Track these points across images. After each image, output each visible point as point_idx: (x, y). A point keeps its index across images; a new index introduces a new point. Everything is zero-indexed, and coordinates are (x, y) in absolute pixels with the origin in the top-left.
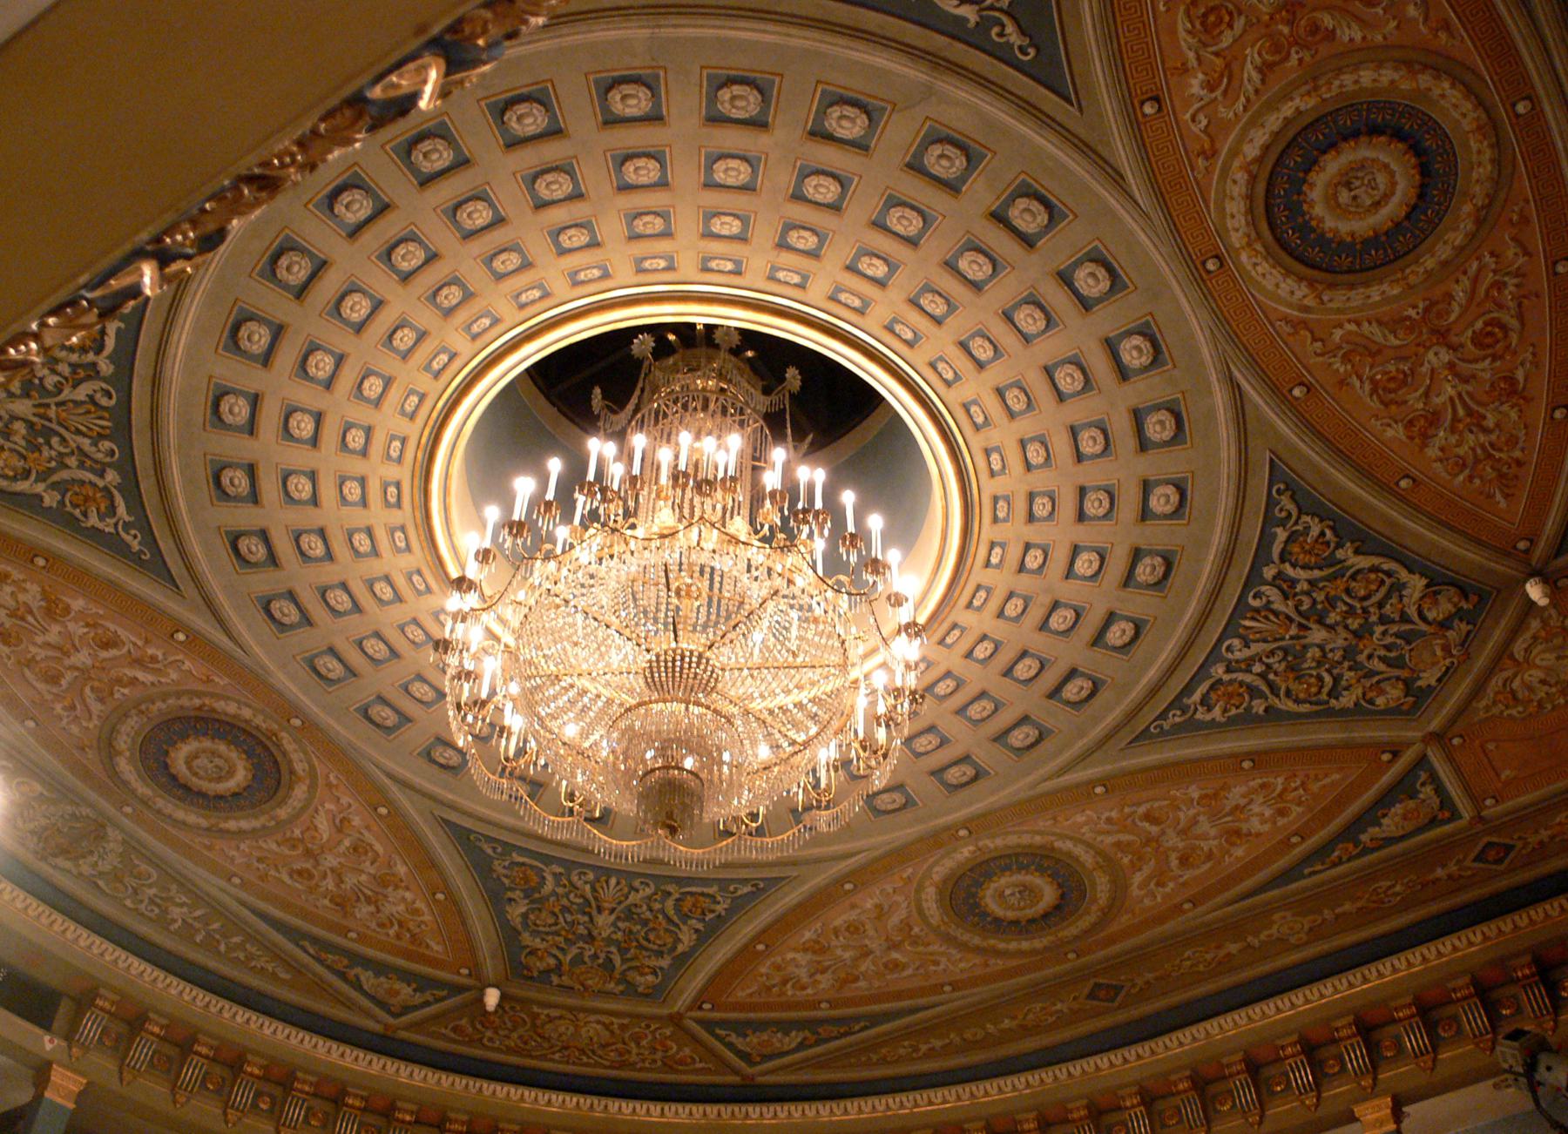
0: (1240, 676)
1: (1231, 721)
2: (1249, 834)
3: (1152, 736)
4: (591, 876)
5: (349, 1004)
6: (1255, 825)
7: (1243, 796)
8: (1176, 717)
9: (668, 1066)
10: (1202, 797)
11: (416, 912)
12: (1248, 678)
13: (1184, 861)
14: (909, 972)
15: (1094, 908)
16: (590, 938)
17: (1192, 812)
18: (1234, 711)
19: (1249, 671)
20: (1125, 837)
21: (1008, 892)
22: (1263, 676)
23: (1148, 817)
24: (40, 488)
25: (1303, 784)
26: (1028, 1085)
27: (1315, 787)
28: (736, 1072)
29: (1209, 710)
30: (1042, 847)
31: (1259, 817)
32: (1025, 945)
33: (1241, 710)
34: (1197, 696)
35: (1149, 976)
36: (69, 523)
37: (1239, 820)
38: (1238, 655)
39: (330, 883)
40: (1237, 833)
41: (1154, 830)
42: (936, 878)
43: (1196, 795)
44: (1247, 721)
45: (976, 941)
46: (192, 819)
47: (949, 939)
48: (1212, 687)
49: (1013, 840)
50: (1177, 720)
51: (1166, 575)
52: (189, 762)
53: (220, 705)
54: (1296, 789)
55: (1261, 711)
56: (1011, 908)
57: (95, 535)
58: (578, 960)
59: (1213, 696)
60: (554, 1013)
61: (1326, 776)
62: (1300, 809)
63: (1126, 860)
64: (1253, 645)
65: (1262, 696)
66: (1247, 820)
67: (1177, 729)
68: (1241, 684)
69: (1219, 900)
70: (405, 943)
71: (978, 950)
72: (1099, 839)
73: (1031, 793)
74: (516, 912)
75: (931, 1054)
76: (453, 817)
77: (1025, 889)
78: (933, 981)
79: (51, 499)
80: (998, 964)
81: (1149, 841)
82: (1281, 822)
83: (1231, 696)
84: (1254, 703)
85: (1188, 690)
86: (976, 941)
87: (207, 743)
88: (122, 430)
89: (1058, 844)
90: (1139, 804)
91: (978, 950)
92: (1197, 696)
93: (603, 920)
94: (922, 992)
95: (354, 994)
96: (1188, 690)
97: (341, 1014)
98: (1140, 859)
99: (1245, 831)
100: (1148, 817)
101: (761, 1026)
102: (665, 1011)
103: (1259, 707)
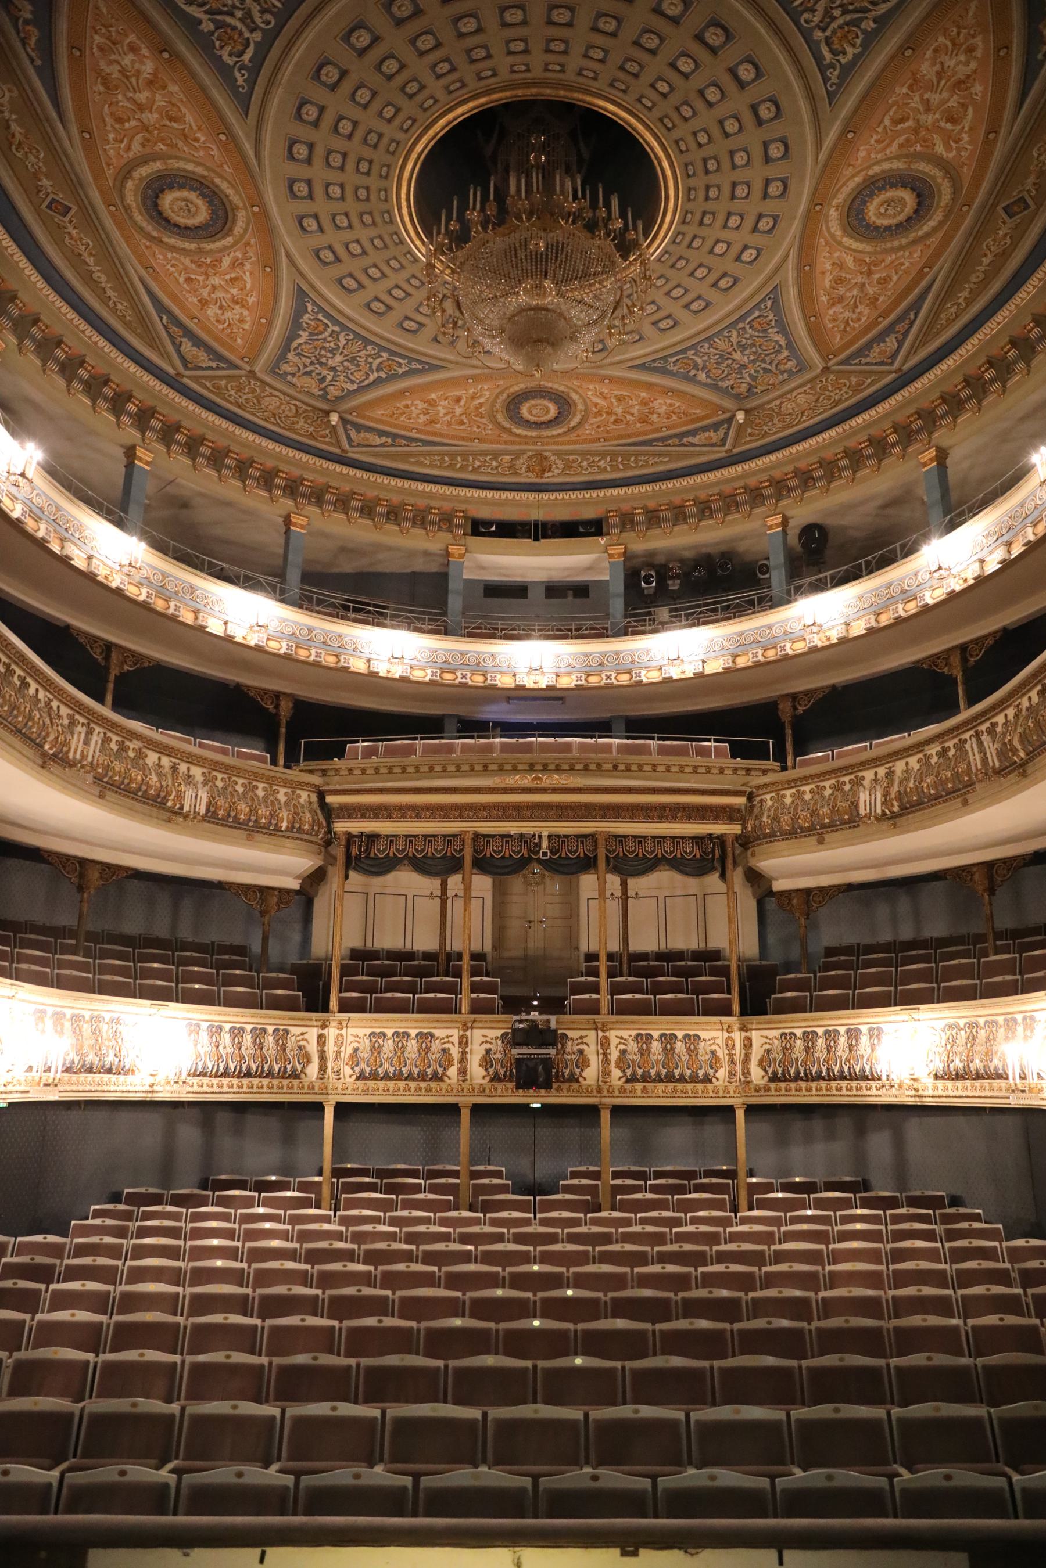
0: (834, 25)
1: (865, 45)
2: (968, 77)
3: (835, 93)
4: (706, 345)
5: (692, 455)
6: (421, 405)
7: (934, 64)
8: (834, 75)
9: (856, 391)
10: (910, 88)
11: (671, 405)
12: (841, 21)
13: (458, 400)
14: (895, 278)
15: (939, 180)
16: (744, 366)
17: (917, 98)
18: (858, 41)
19: (834, 19)
20: (901, 140)
21: (882, 210)
22: (845, 12)
23: (896, 122)
24: (376, 375)
25: (959, 27)
26: (1040, 280)
27: (970, 19)
28: (891, 372)
29: (844, 53)
30: (864, 180)
31: (959, 65)
32: (932, 223)
33: (861, 37)
34: (828, 56)
35: (1031, 179)
36: (393, 377)
37: (950, 77)
38: (816, 20)
39: (629, 418)
40: (960, 82)
41: (910, 123)
42: (839, 233)
43: (905, 90)
44: (870, 40)
45: (904, 241)
46: (560, 431)
47: (886, 251)
48: (828, 44)
49: (846, 190)
50: (836, 73)
51: (724, 28)
52: (530, 413)
53: (512, 390)
54: (958, 34)
55: (872, 25)
56: (894, 216)
57: (405, 374)
58: (754, 378)
59: (836, 46)
60: (778, 402)
61: (967, 10)
62: (979, 38)
63: (918, 148)
64: (817, 7)
65: (861, 19)
66: (955, 73)
67: (842, 77)
68: (841, 27)
69: (1007, 115)
70: (684, 419)
71: (915, 242)
72: (888, 152)
73: (820, 166)
74: (702, 376)
75: (969, 302)
76: (630, 364)
77: (888, 202)
78: (913, 273)
79: (383, 375)
80: (934, 241)
81: (916, 131)
82: (978, 53)
83: (845, 37)
84: (863, 26)
85: (818, 58)
86: (904, 241)
87: (533, 402)
88: (367, 342)
89: (871, 173)
90: (882, 121)
91: (915, 242)
92: (828, 56)
93: (737, 356)
94: (915, 282)
95: (692, 449)
96: (818, 58)
97: (703, 459)
98: (925, 141)
99: (963, 78)
100: (896, 122)
101: (869, 346)
102: (818, 371)
103: (869, 25)
